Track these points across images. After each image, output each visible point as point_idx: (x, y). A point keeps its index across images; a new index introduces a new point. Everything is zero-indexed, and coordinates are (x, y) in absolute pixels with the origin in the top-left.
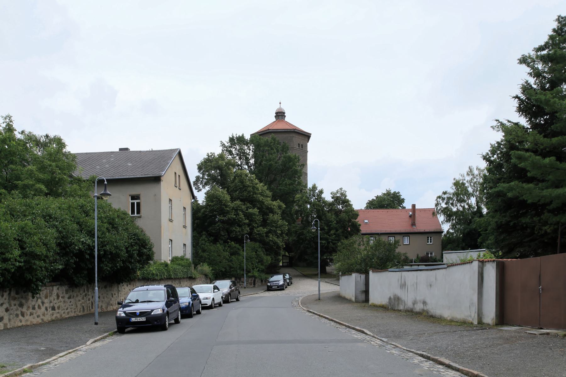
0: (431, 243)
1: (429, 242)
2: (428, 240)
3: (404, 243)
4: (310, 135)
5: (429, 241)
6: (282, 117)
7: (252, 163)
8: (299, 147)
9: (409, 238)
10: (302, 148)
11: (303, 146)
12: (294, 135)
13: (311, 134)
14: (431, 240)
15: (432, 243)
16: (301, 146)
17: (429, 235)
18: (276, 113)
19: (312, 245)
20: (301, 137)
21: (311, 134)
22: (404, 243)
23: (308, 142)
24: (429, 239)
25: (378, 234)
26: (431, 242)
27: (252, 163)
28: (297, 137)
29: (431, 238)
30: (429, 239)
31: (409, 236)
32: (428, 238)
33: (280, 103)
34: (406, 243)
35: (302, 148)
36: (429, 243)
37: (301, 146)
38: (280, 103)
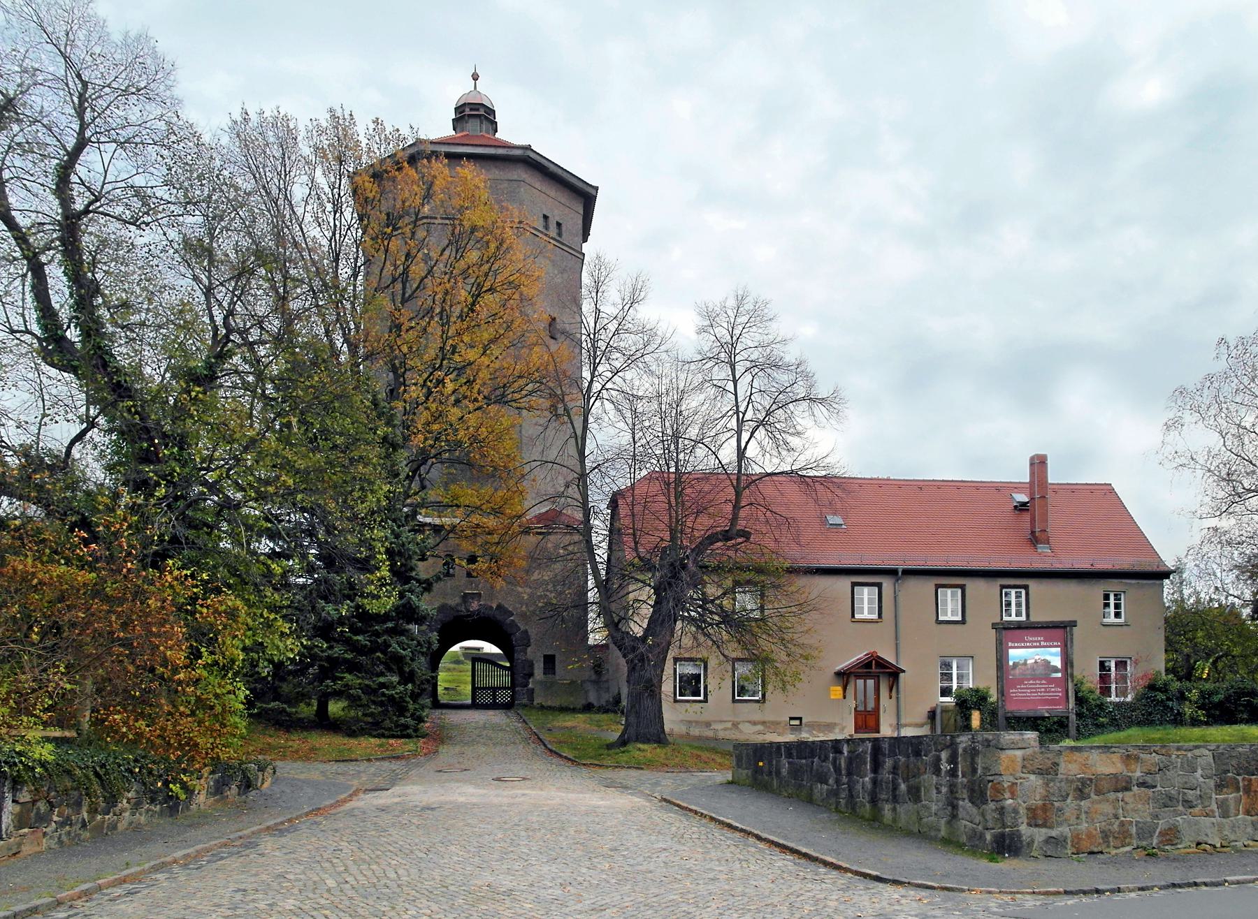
0: (1118, 620)
1: (1112, 615)
2: (1107, 605)
3: (941, 618)
4: (593, 192)
5: (1112, 610)
6: (481, 123)
7: (527, 505)
8: (547, 227)
9: (1027, 594)
10: (560, 234)
11: (564, 228)
12: (520, 173)
13: (596, 188)
14: (1117, 606)
15: (1121, 620)
16: (553, 226)
17: (1113, 586)
18: (459, 109)
19: (407, 669)
20: (553, 193)
21: (596, 188)
22: (941, 618)
23: (585, 240)
24: (1112, 601)
25: (891, 572)
26: (1117, 615)
27: (527, 505)
28: (537, 185)
29: (1117, 597)
30: (1112, 601)
31: (1026, 587)
32: (1107, 597)
33: (475, 77)
34: (949, 617)
35: (560, 234)
36: (1112, 619)
37: (553, 226)
38: (475, 77)
